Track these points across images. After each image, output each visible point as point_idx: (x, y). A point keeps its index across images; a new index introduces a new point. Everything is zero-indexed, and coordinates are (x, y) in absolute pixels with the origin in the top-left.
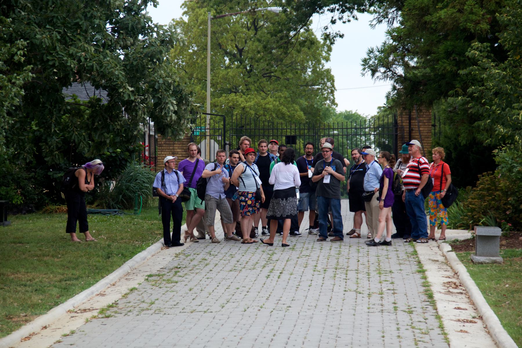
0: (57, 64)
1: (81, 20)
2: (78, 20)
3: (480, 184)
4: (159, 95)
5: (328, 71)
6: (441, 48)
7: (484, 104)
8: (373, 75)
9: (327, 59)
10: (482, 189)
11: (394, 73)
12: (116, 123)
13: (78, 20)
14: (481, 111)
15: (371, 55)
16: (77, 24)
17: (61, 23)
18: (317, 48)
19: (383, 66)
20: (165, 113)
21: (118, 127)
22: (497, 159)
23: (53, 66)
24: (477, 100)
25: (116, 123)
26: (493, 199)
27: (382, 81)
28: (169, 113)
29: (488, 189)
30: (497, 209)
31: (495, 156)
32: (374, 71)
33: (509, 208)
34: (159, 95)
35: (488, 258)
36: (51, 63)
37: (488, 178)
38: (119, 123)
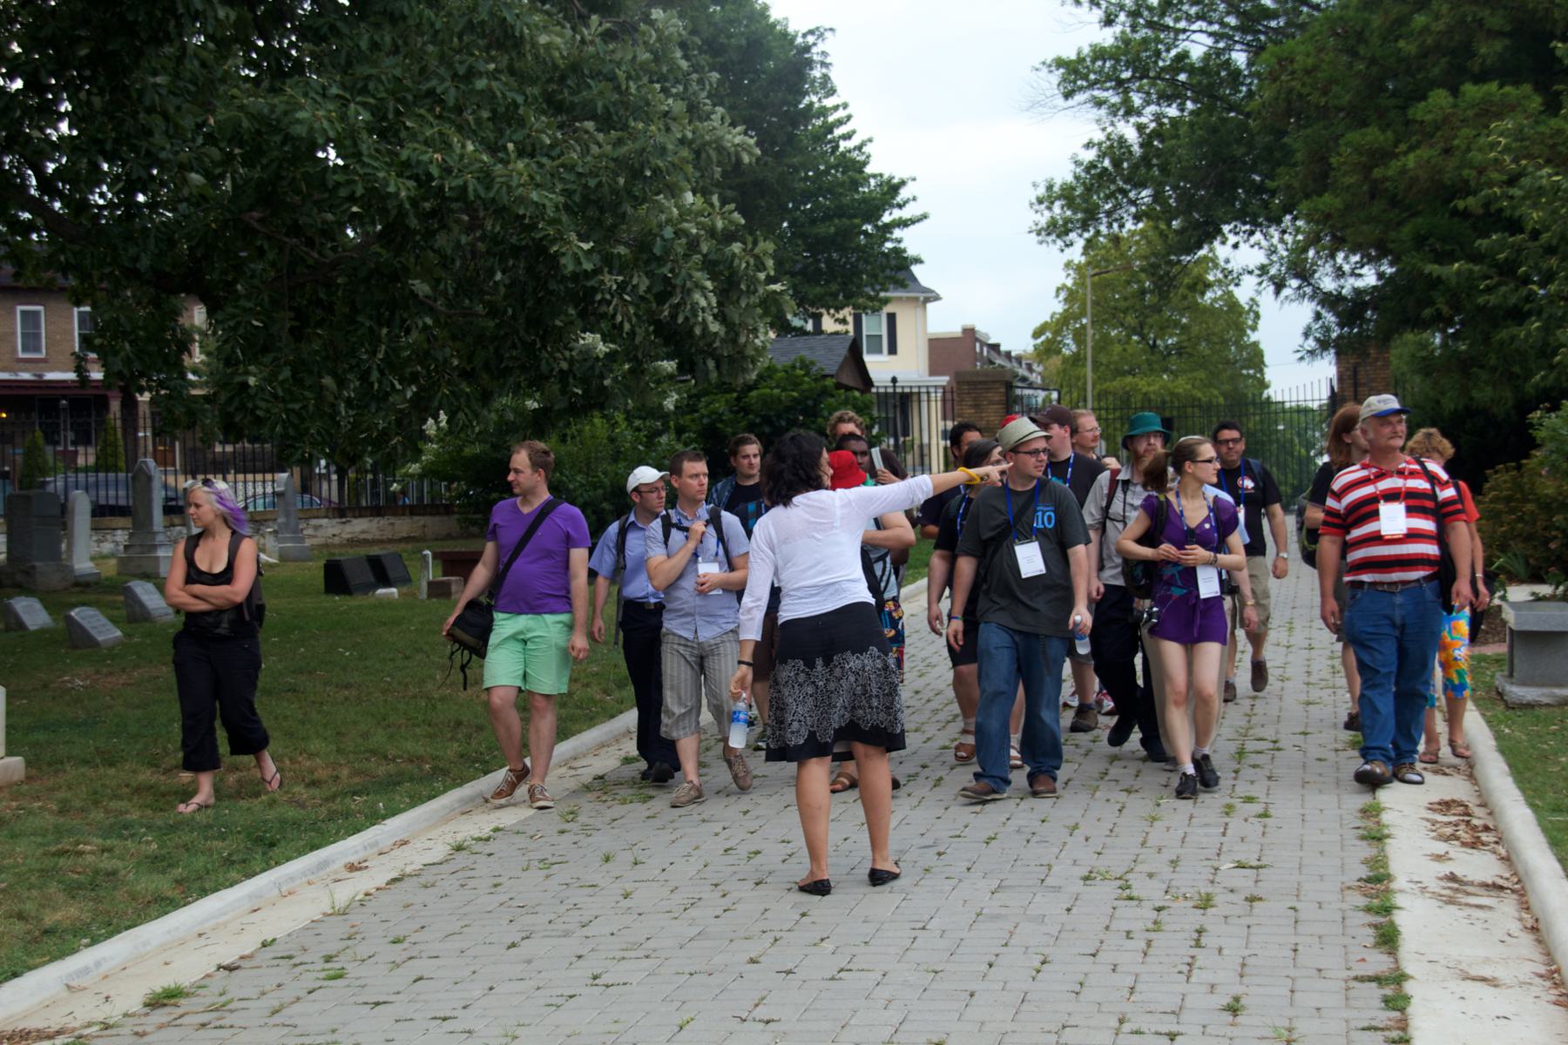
0: (360, 191)
1: (442, 80)
2: (434, 83)
3: (1492, 489)
4: (665, 270)
5: (1256, 344)
6: (1407, 231)
7: (1526, 281)
8: (1277, 292)
9: (1254, 329)
10: (1494, 500)
11: (1316, 289)
12: (558, 355)
13: (434, 83)
14: (1513, 300)
15: (1274, 258)
16: (431, 93)
17: (386, 91)
18: (1240, 314)
19: (1296, 276)
20: (687, 319)
21: (564, 365)
22: (1541, 434)
23: (352, 199)
24: (1507, 270)
25: (558, 355)
26: (1520, 519)
27: (1295, 304)
28: (696, 316)
29: (1508, 499)
30: (1528, 538)
31: (1531, 425)
32: (1279, 286)
33: (1555, 537)
34: (665, 270)
35: (1546, 690)
36: (343, 193)
37: (1506, 477)
38: (567, 353)
